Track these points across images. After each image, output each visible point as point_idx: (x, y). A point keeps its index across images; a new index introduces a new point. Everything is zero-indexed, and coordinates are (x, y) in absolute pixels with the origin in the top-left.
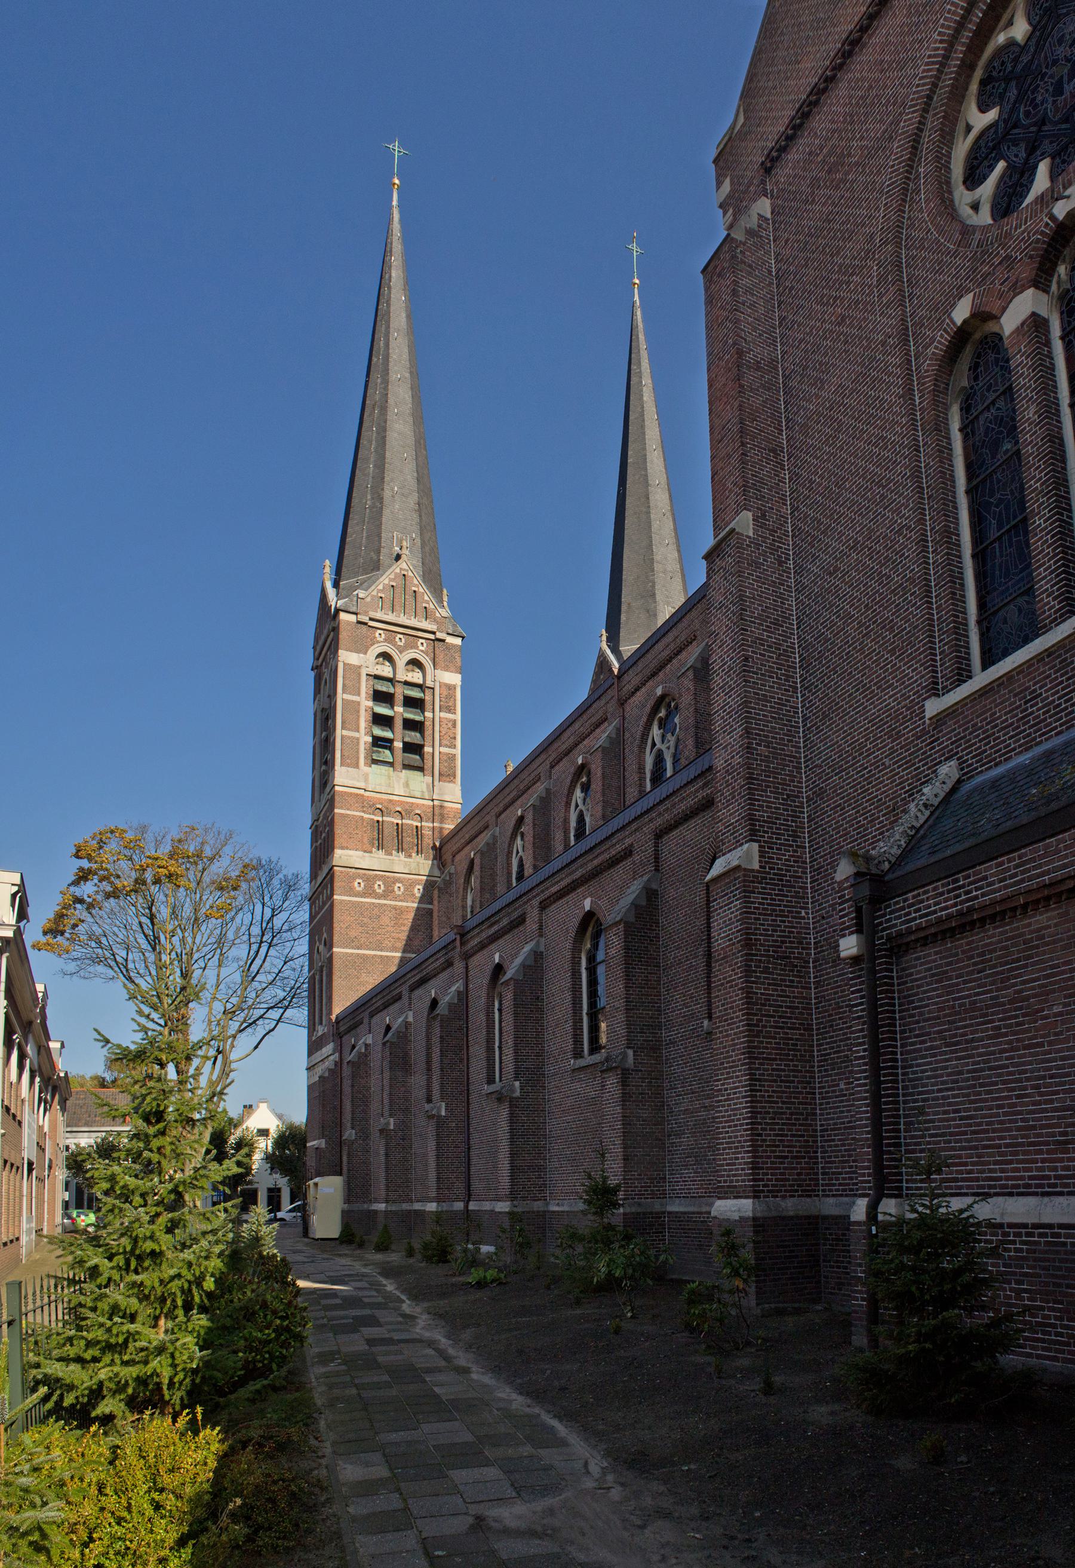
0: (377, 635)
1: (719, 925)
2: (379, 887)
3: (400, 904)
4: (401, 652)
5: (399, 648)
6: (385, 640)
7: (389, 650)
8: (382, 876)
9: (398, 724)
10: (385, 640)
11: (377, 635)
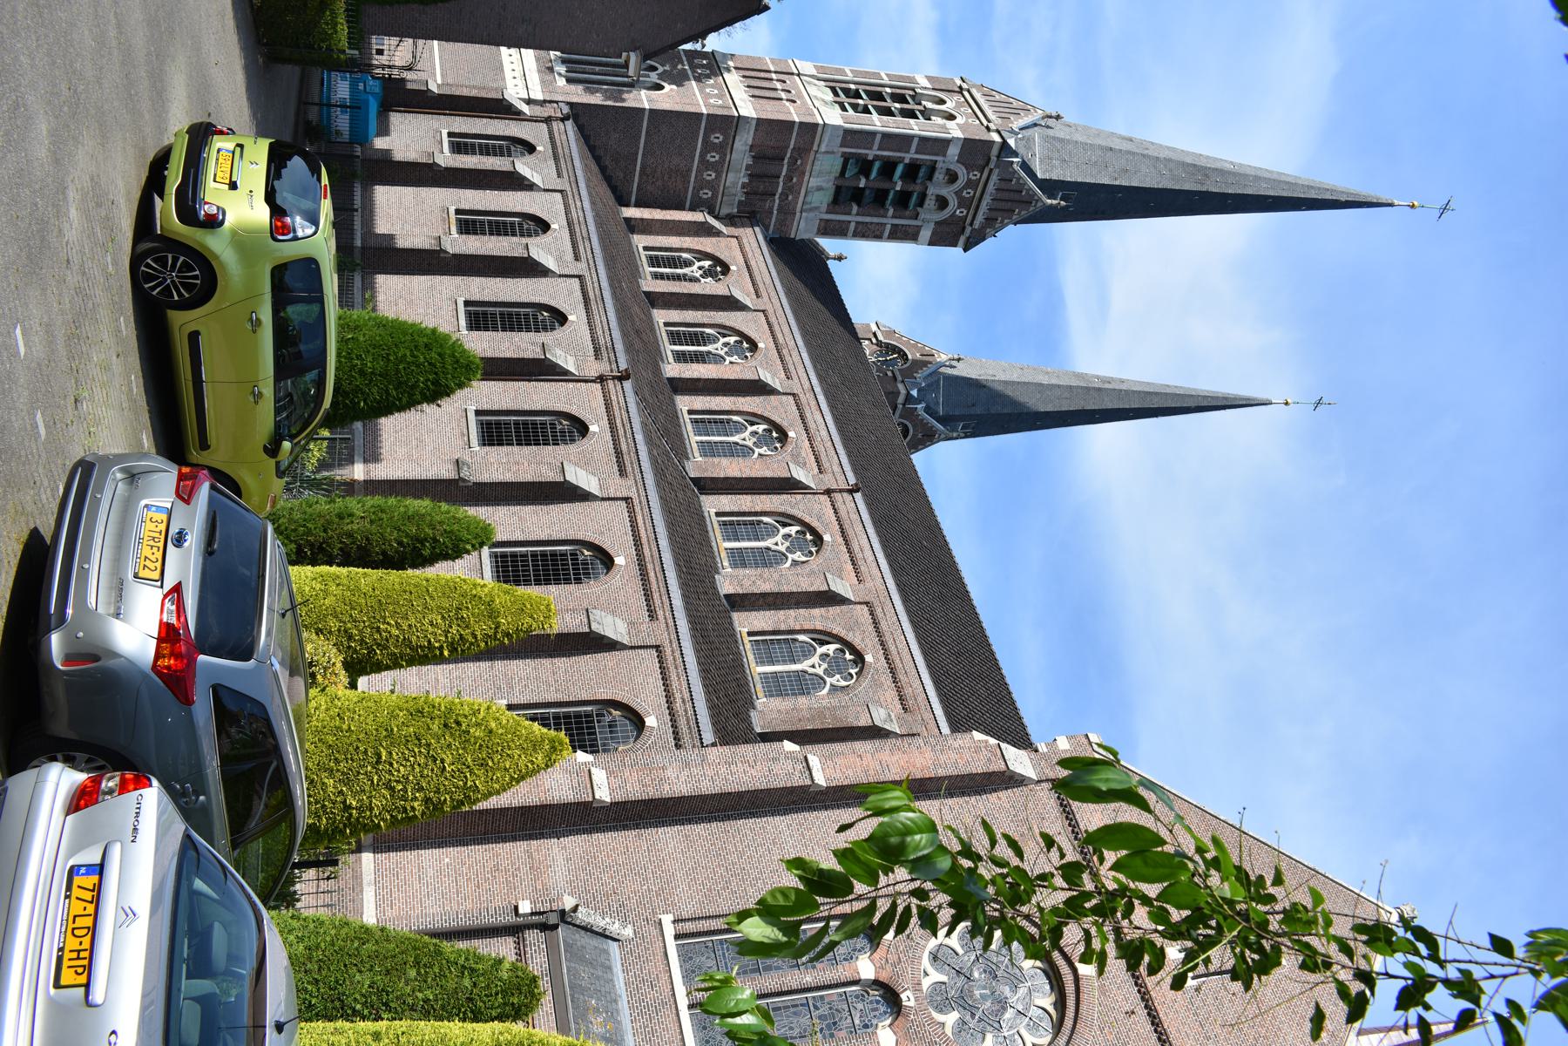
2: (713, 157)
5: (961, 191)
6: (969, 180)
9: (884, 185)
10: (969, 180)
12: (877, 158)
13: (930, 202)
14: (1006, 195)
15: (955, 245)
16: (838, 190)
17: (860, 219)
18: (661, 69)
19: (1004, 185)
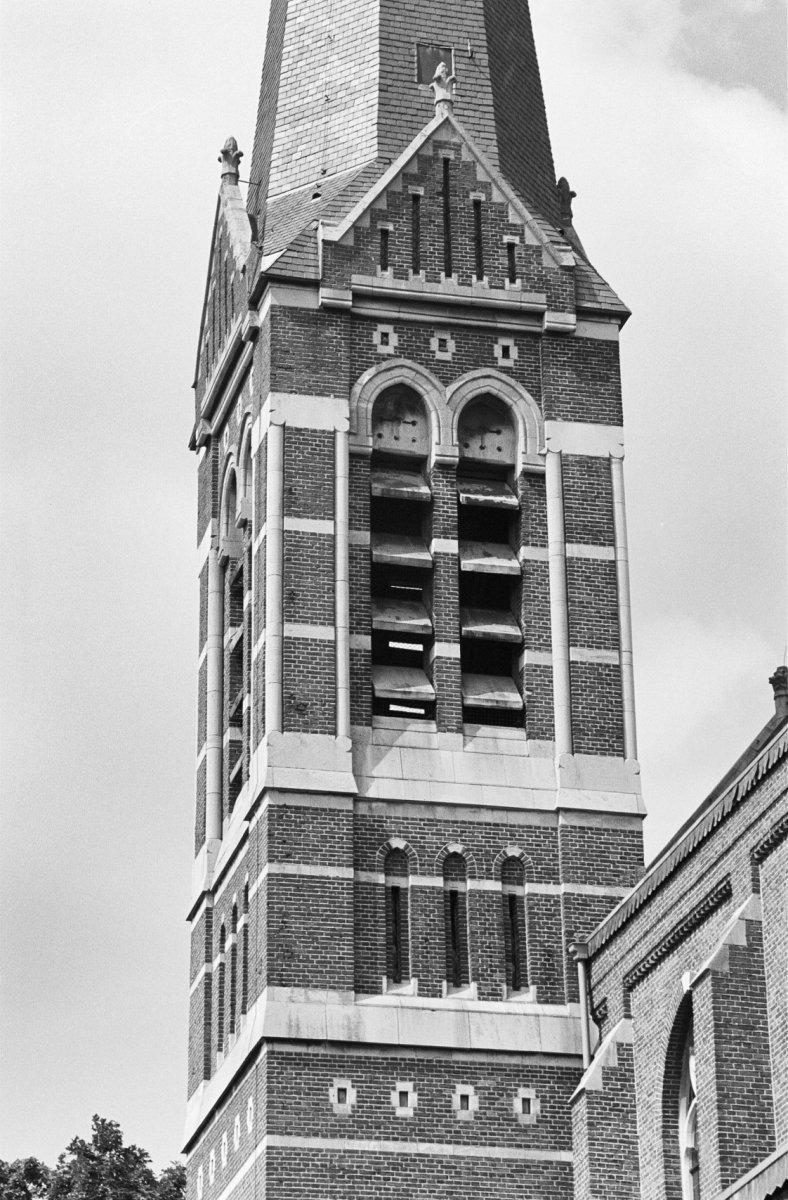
10: (401, 351)
14: (432, 245)
15: (614, 346)
19: (402, 254)
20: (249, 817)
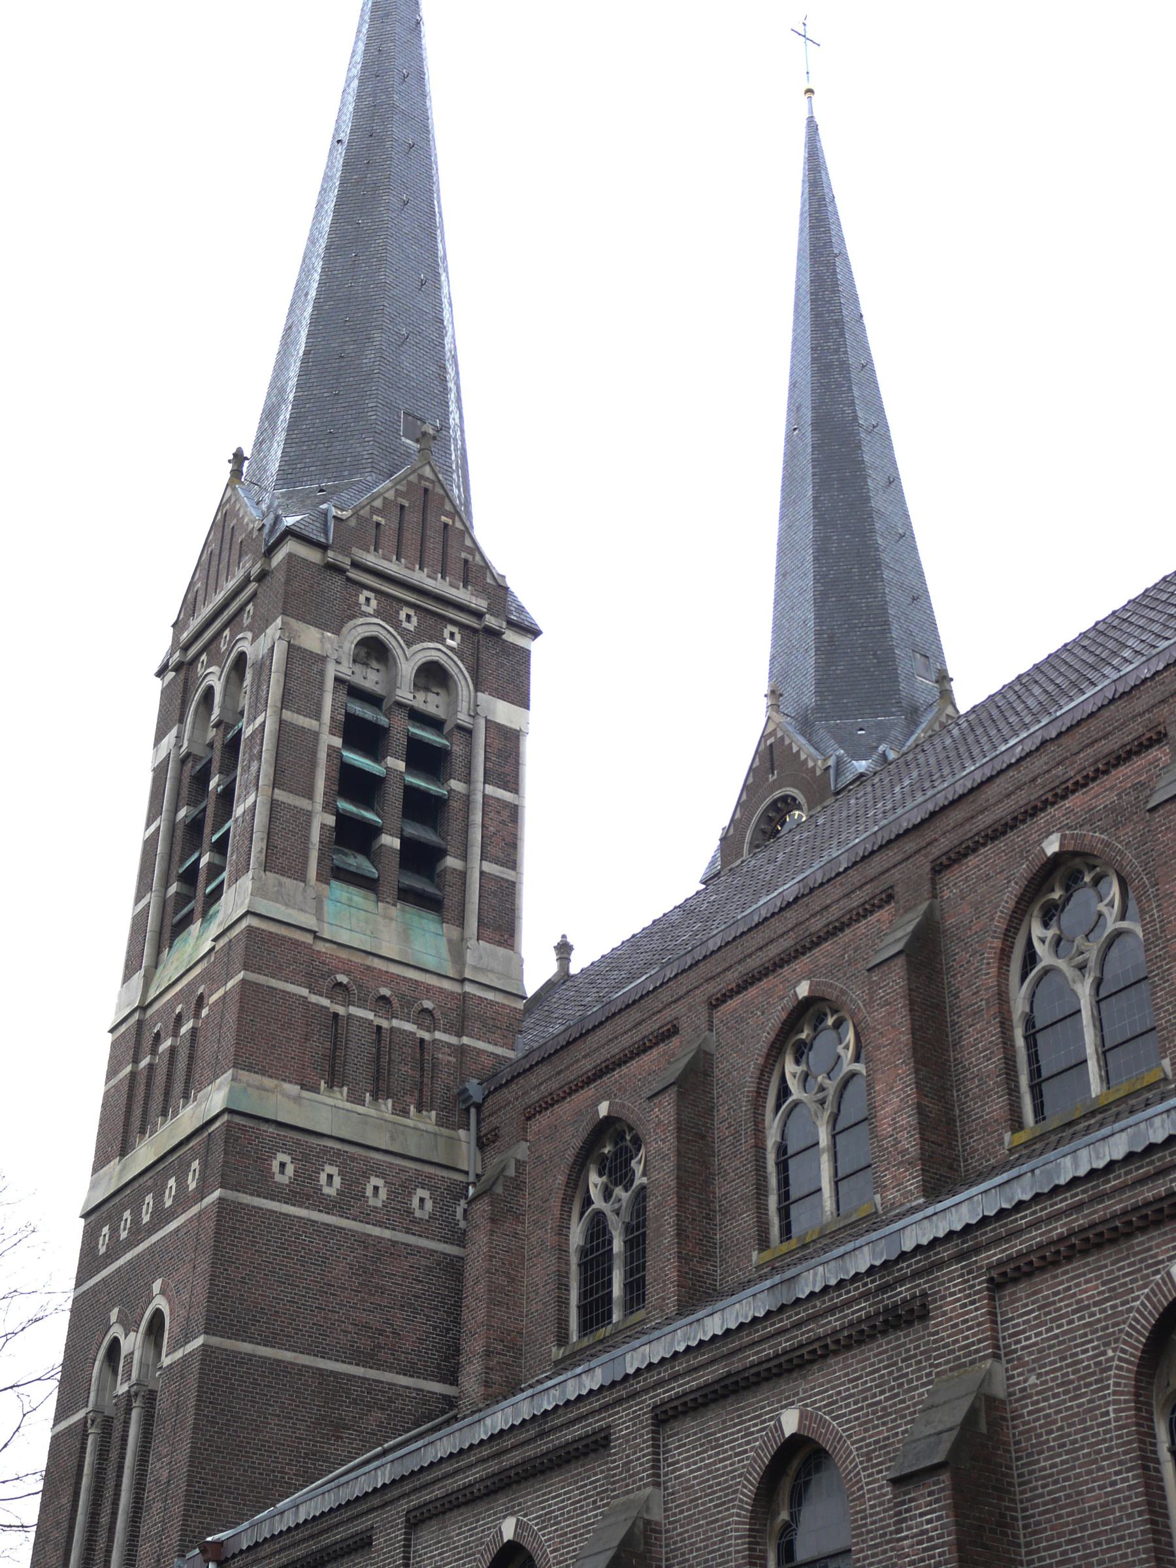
0: (362, 599)
1: (642, 1436)
3: (376, 1231)
4: (409, 644)
5: (404, 633)
6: (378, 614)
7: (383, 635)
8: (339, 1153)
10: (378, 614)
11: (362, 599)
12: (328, 806)
13: (431, 703)
15: (525, 654)
16: (406, 895)
17: (476, 851)
18: (116, 1331)
19: (389, 539)
20: (215, 940)
